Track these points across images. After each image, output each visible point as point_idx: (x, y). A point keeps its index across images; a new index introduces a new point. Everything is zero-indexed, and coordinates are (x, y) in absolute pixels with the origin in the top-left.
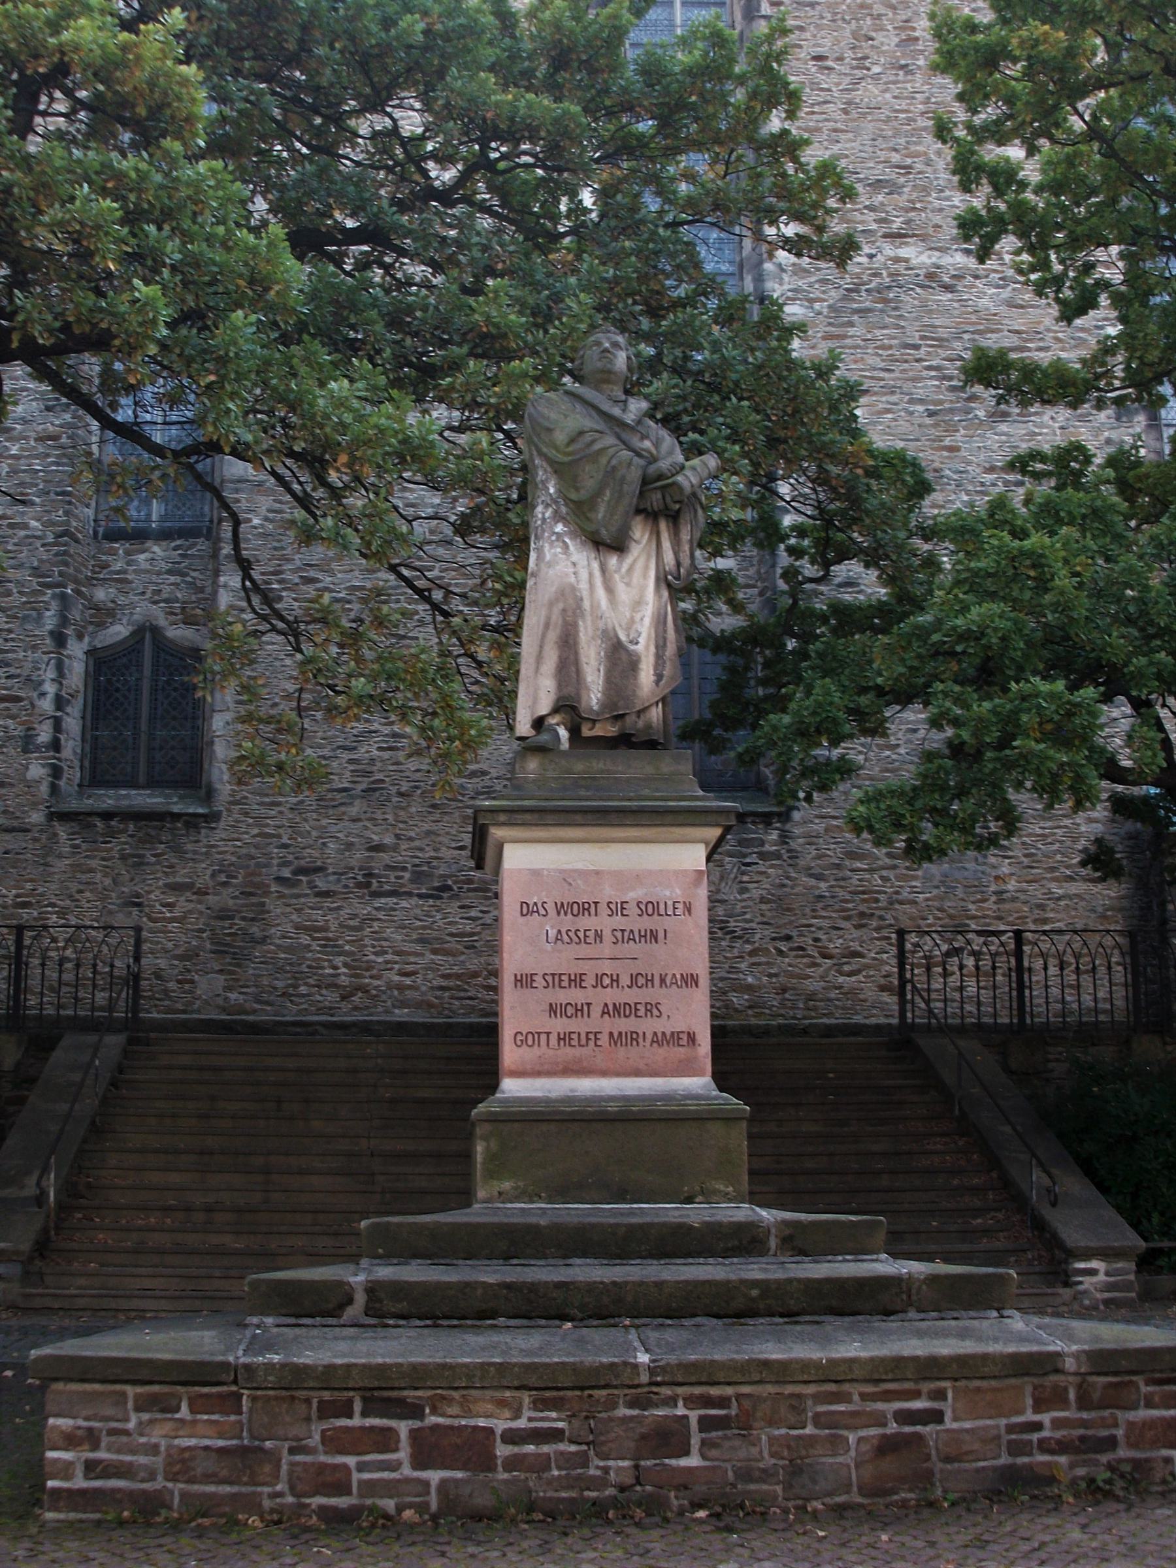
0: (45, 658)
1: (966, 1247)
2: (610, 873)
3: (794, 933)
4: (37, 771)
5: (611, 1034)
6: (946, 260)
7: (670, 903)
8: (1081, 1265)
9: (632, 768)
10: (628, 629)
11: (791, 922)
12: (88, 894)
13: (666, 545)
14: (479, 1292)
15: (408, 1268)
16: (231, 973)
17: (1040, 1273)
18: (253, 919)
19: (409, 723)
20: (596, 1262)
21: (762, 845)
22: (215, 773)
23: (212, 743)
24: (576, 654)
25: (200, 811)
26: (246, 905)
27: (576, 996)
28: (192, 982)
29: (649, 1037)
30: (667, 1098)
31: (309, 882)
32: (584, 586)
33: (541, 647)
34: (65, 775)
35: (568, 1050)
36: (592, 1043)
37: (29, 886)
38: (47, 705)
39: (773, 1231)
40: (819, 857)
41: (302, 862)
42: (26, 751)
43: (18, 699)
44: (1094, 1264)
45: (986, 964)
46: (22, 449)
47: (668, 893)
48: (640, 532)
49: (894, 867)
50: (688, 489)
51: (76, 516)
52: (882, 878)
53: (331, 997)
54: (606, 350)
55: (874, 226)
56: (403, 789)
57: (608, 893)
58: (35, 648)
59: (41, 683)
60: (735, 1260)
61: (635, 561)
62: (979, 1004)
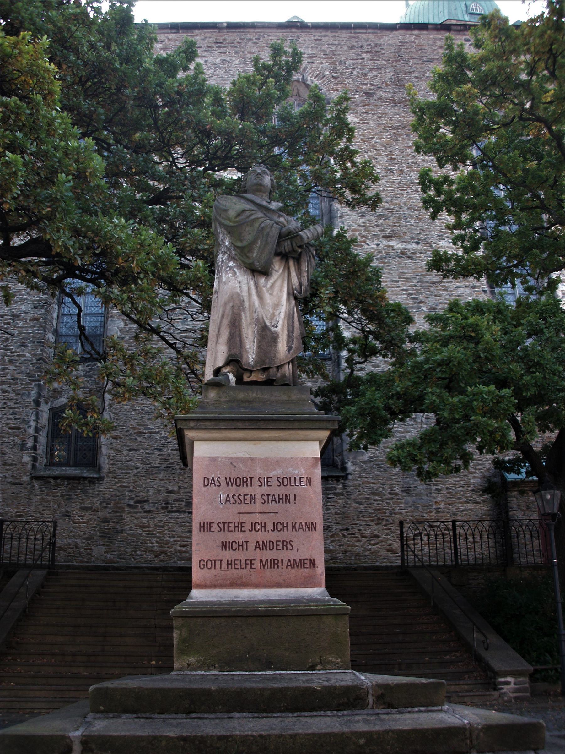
0: (31, 411)
1: (443, 671)
2: (260, 459)
3: (350, 527)
4: (26, 459)
5: (261, 560)
6: (409, 246)
7: (298, 478)
8: (502, 680)
9: (274, 397)
10: (271, 319)
11: (348, 523)
12: (47, 511)
13: (294, 274)
14: (164, 743)
15: (120, 721)
16: (107, 545)
17: (481, 684)
18: (117, 523)
19: (158, 401)
20: (250, 715)
21: (336, 489)
22: (102, 459)
23: (101, 447)
24: (240, 331)
25: (95, 476)
27: (239, 536)
28: (91, 549)
29: (285, 562)
30: (297, 601)
32: (245, 294)
33: (219, 329)
34: (39, 461)
35: (234, 571)
36: (249, 566)
37: (22, 508)
38: (31, 431)
39: (371, 691)
40: (360, 495)
41: (139, 498)
42: (22, 450)
43: (19, 428)
44: (509, 679)
45: (432, 539)
46: (24, 324)
47: (296, 472)
48: (278, 267)
49: (392, 499)
50: (306, 240)
51: (46, 352)
52: (387, 503)
53: (151, 556)
54: (259, 174)
55: (379, 233)
57: (259, 472)
58: (27, 407)
59: (29, 422)
60: (345, 712)
61: (275, 282)
62: (430, 556)
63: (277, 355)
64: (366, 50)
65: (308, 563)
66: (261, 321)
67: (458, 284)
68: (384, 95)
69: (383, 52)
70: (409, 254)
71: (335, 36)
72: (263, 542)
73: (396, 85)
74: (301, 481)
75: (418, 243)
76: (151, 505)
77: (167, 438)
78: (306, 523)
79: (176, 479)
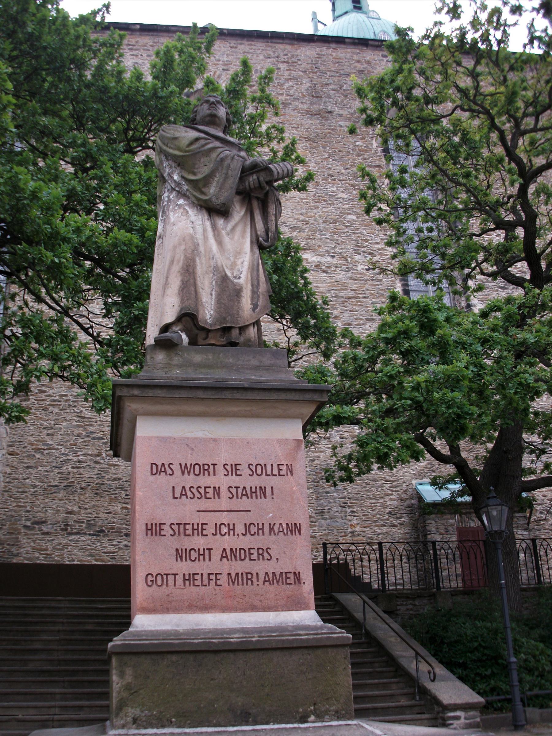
6: (323, 260)
18: (13, 545)
24: (195, 279)
26: (8, 539)
27: (198, 542)
29: (262, 577)
30: (281, 629)
31: (39, 528)
32: (199, 236)
33: (167, 278)
36: (213, 583)
48: (238, 212)
54: (213, 103)
56: (83, 486)
57: (224, 456)
63: (240, 312)
64: (283, 60)
65: (292, 578)
66: (221, 269)
67: (374, 300)
68: (300, 106)
69: (300, 63)
70: (323, 268)
71: (251, 45)
72: (232, 549)
73: (313, 96)
74: (279, 470)
75: (333, 257)
76: (50, 526)
77: (67, 455)
78: (287, 524)
79: (77, 498)
